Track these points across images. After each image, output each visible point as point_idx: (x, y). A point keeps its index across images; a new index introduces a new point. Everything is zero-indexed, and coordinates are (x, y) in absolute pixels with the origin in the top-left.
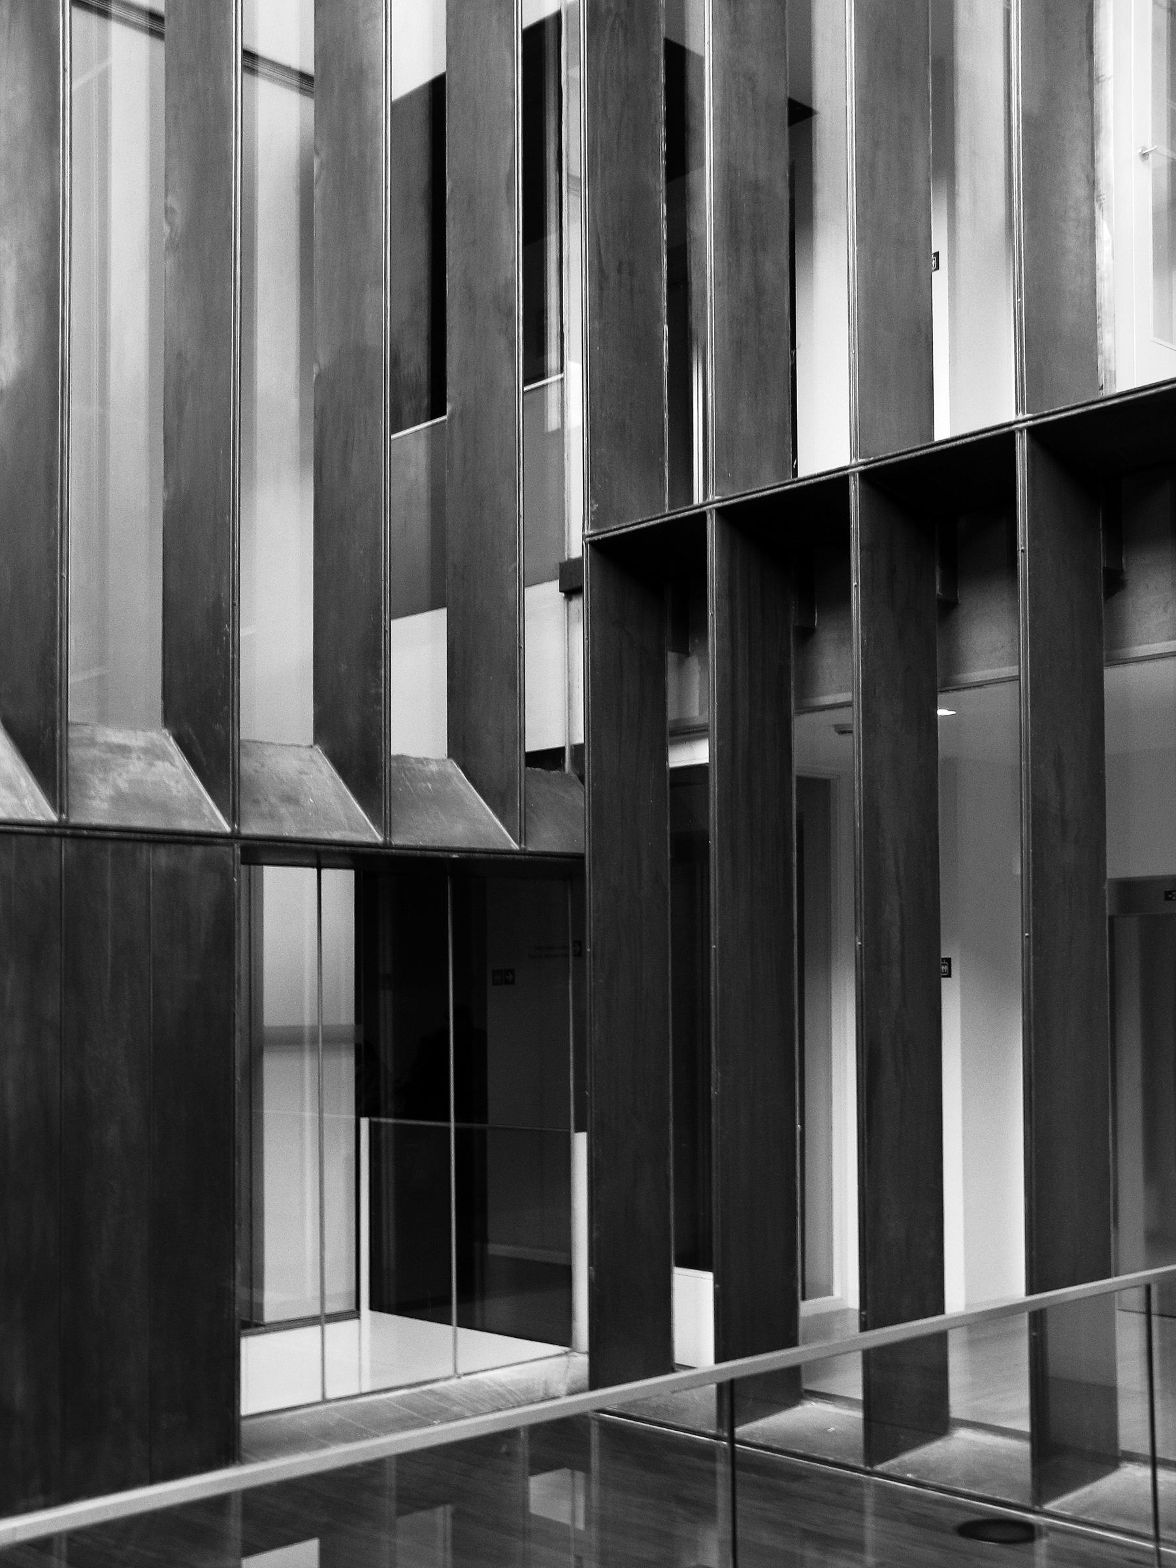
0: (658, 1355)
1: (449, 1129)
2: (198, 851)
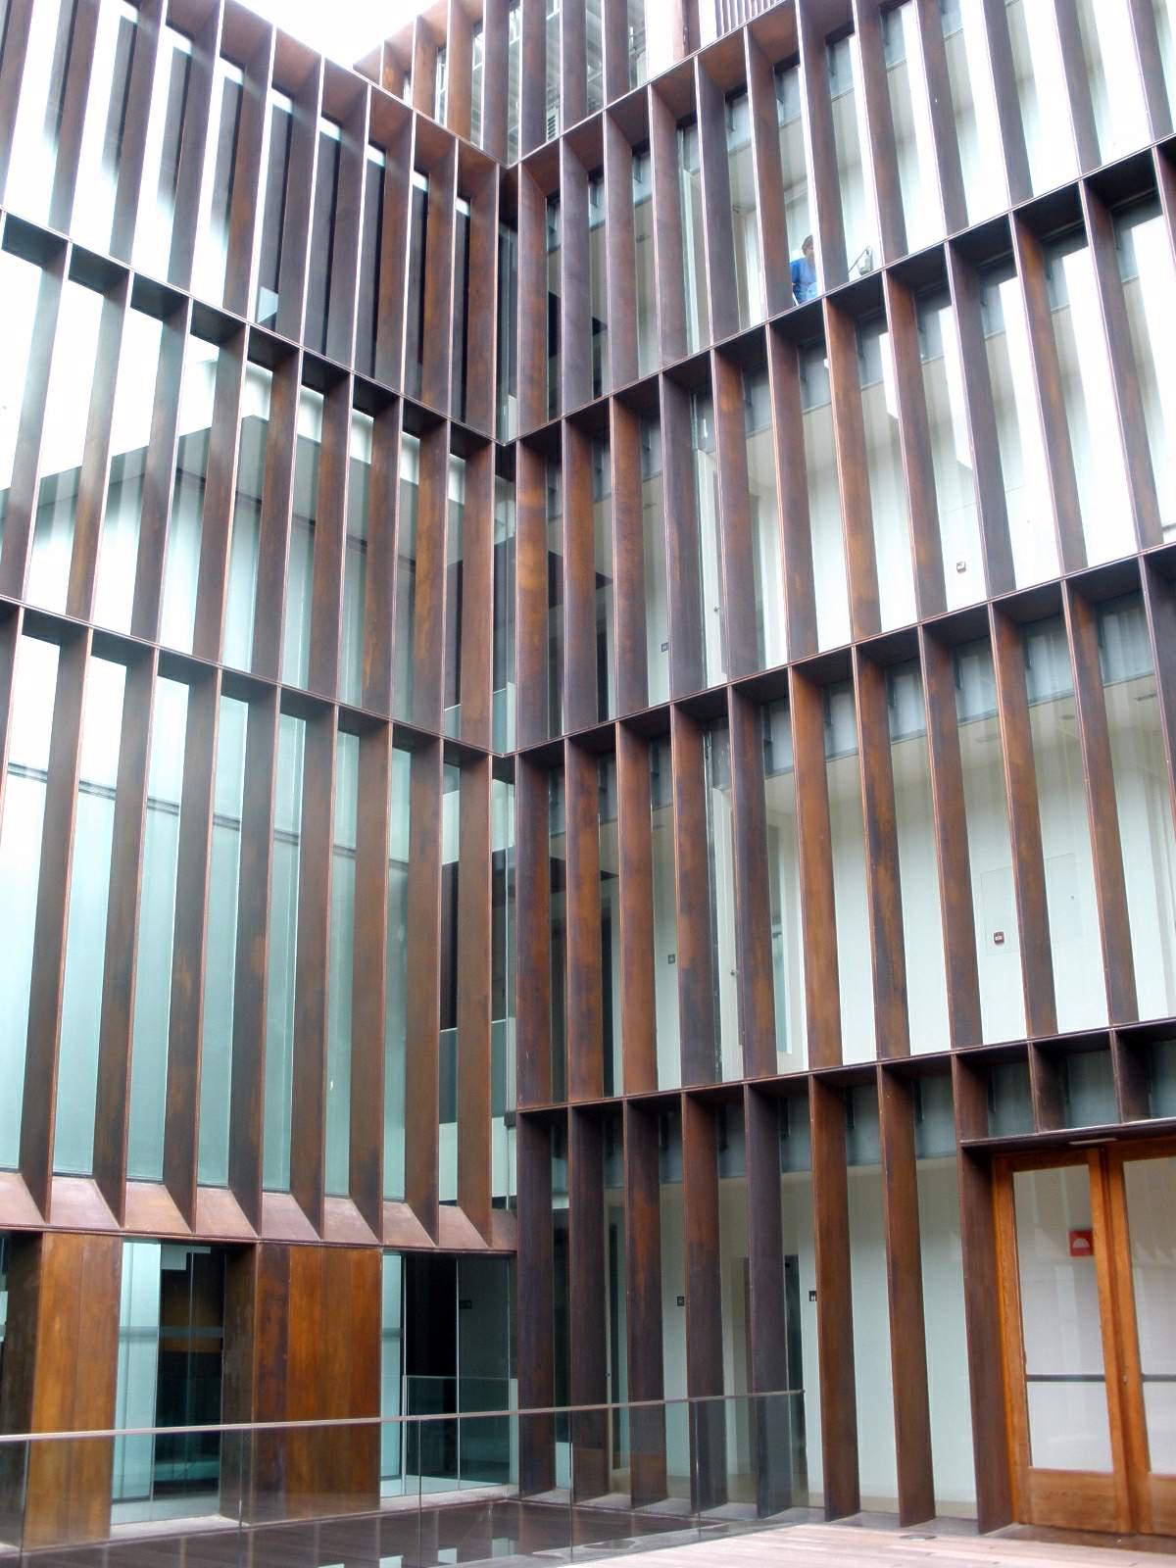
0: (549, 1483)
1: (455, 1381)
2: (368, 1252)
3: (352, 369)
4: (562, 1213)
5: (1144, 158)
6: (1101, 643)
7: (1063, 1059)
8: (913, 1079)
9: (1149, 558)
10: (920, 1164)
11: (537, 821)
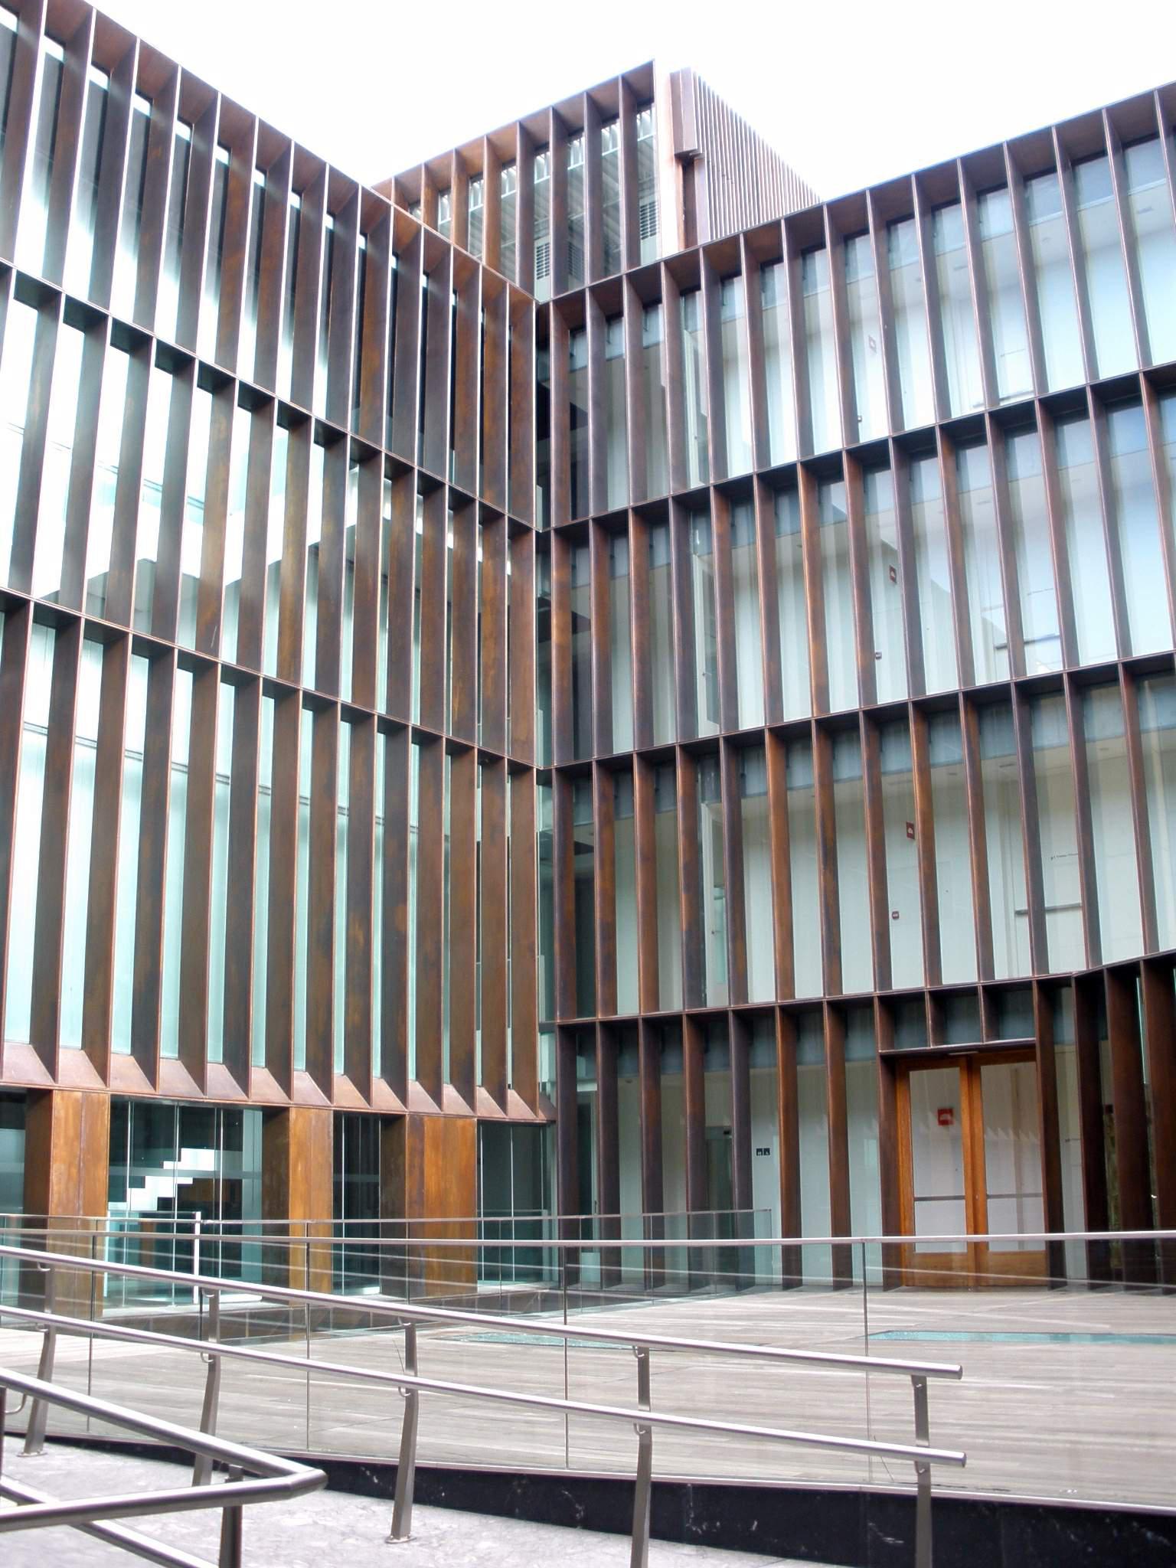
3: (447, 481)
4: (587, 1094)
5: (1029, 405)
6: (980, 732)
7: (948, 1002)
8: (848, 1012)
9: (1017, 684)
10: (752, 1071)
11: (566, 818)
